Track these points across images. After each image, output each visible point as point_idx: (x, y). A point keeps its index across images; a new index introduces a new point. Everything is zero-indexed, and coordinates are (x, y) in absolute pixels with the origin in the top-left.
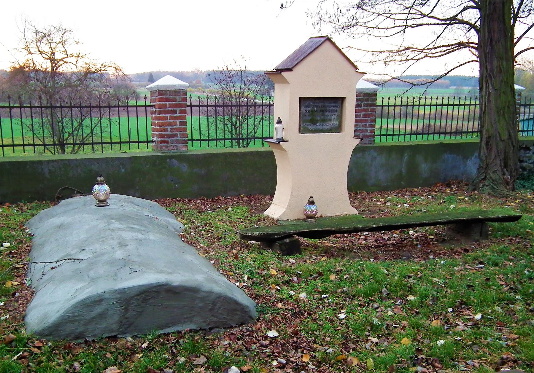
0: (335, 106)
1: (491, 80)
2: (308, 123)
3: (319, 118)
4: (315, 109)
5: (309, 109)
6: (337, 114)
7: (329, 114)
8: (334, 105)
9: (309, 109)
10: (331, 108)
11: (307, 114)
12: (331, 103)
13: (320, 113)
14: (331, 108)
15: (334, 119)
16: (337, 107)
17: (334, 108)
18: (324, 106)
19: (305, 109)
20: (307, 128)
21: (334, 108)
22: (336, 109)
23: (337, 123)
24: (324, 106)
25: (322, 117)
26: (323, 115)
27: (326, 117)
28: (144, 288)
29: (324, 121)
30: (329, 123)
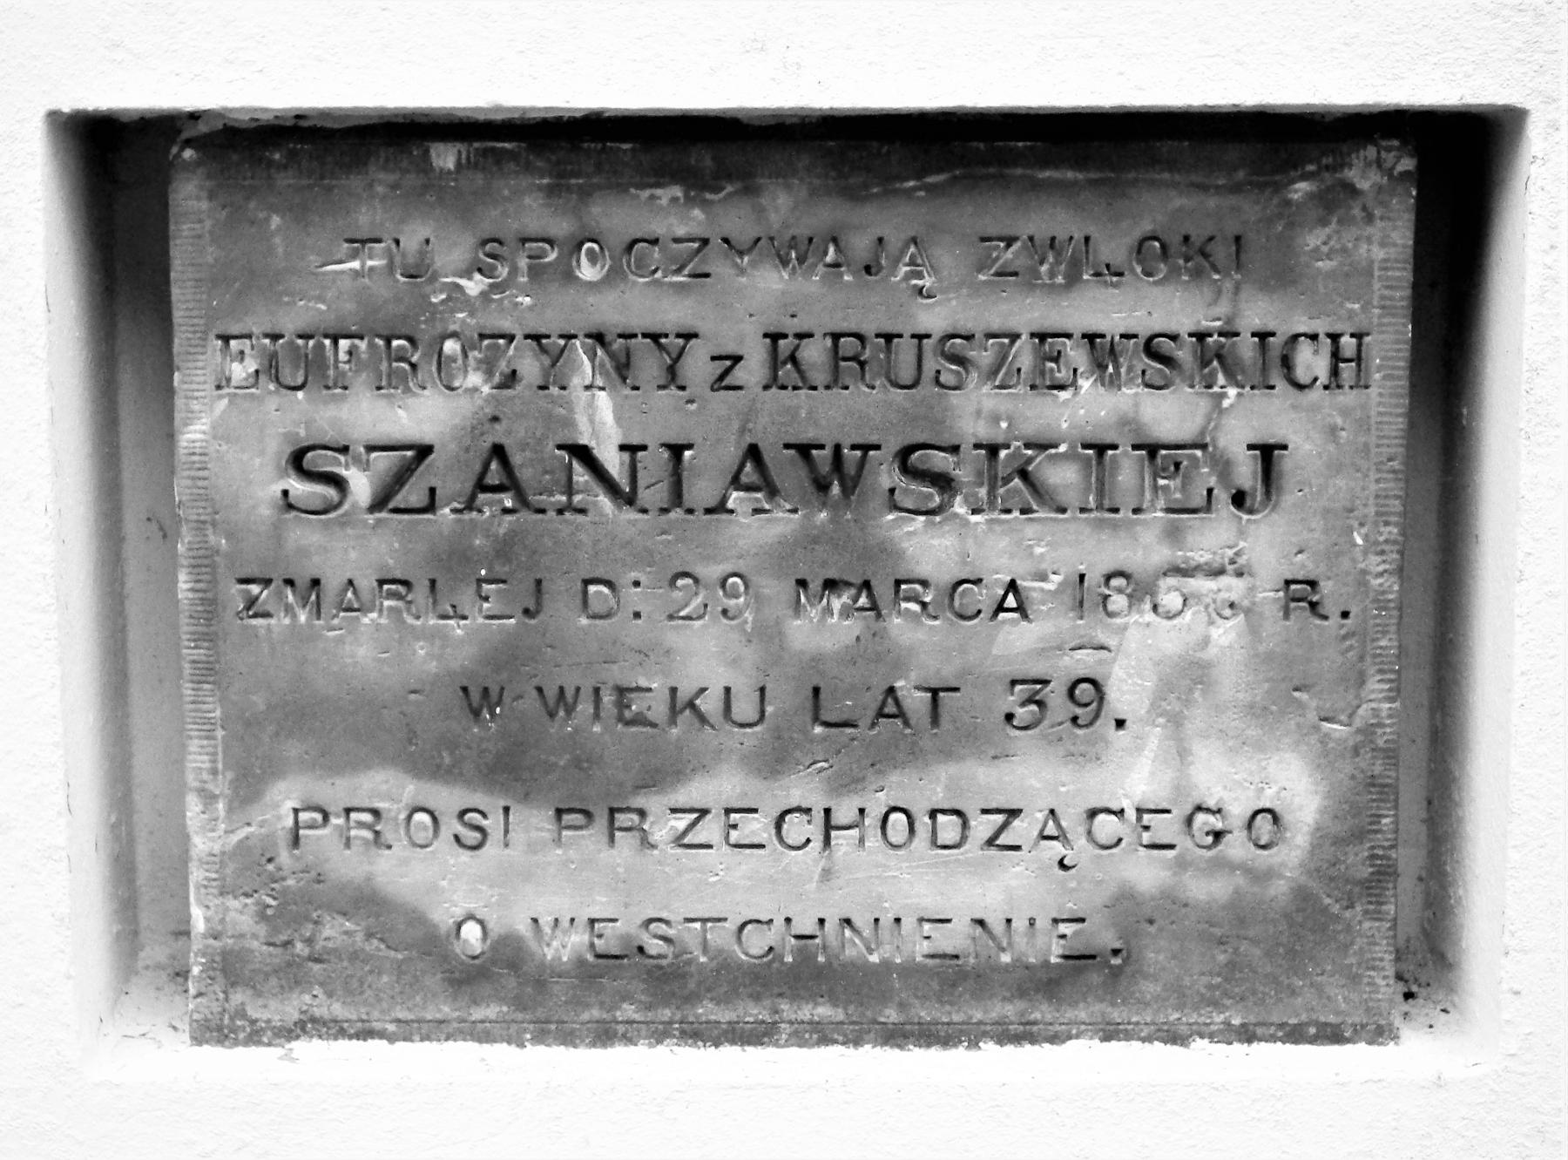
0: (1213, 355)
1: (200, 738)
2: (387, 787)
3: (705, 657)
4: (601, 418)
5: (424, 414)
6: (1269, 545)
7: (1042, 549)
8: (1174, 309)
9: (424, 414)
10: (1087, 405)
11: (353, 551)
12: (1077, 265)
13: (757, 529)
14: (1087, 405)
15: (1188, 679)
16: (1275, 361)
17: (1170, 413)
18: (852, 355)
19: (296, 414)
20: (366, 902)
21: (1170, 413)
22: (1244, 418)
23: (1297, 787)
24: (852, 355)
25: (825, 629)
26: (872, 586)
27: (920, 642)
28: (363, 122)
29: (861, 725)
30: (1034, 775)
